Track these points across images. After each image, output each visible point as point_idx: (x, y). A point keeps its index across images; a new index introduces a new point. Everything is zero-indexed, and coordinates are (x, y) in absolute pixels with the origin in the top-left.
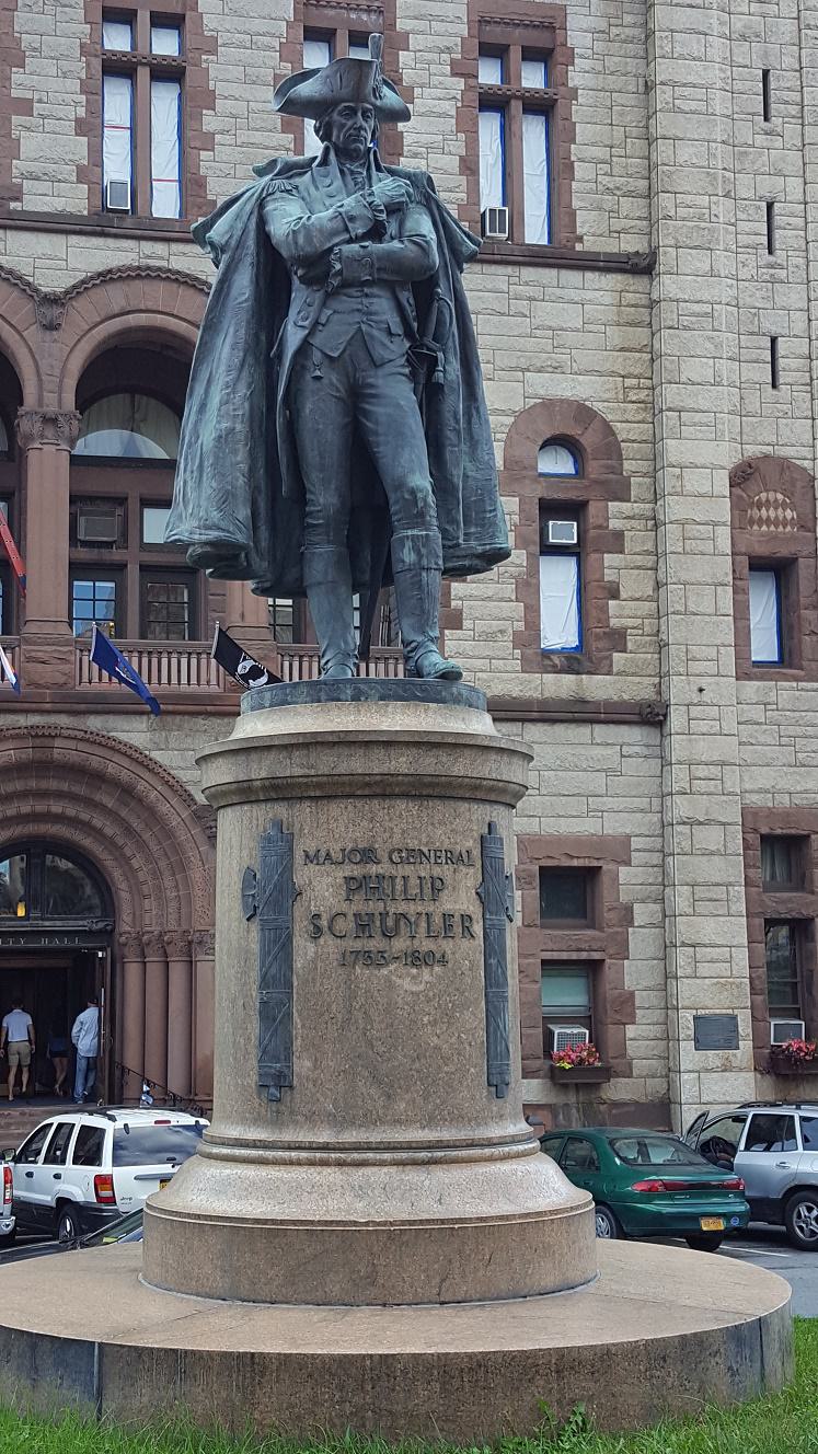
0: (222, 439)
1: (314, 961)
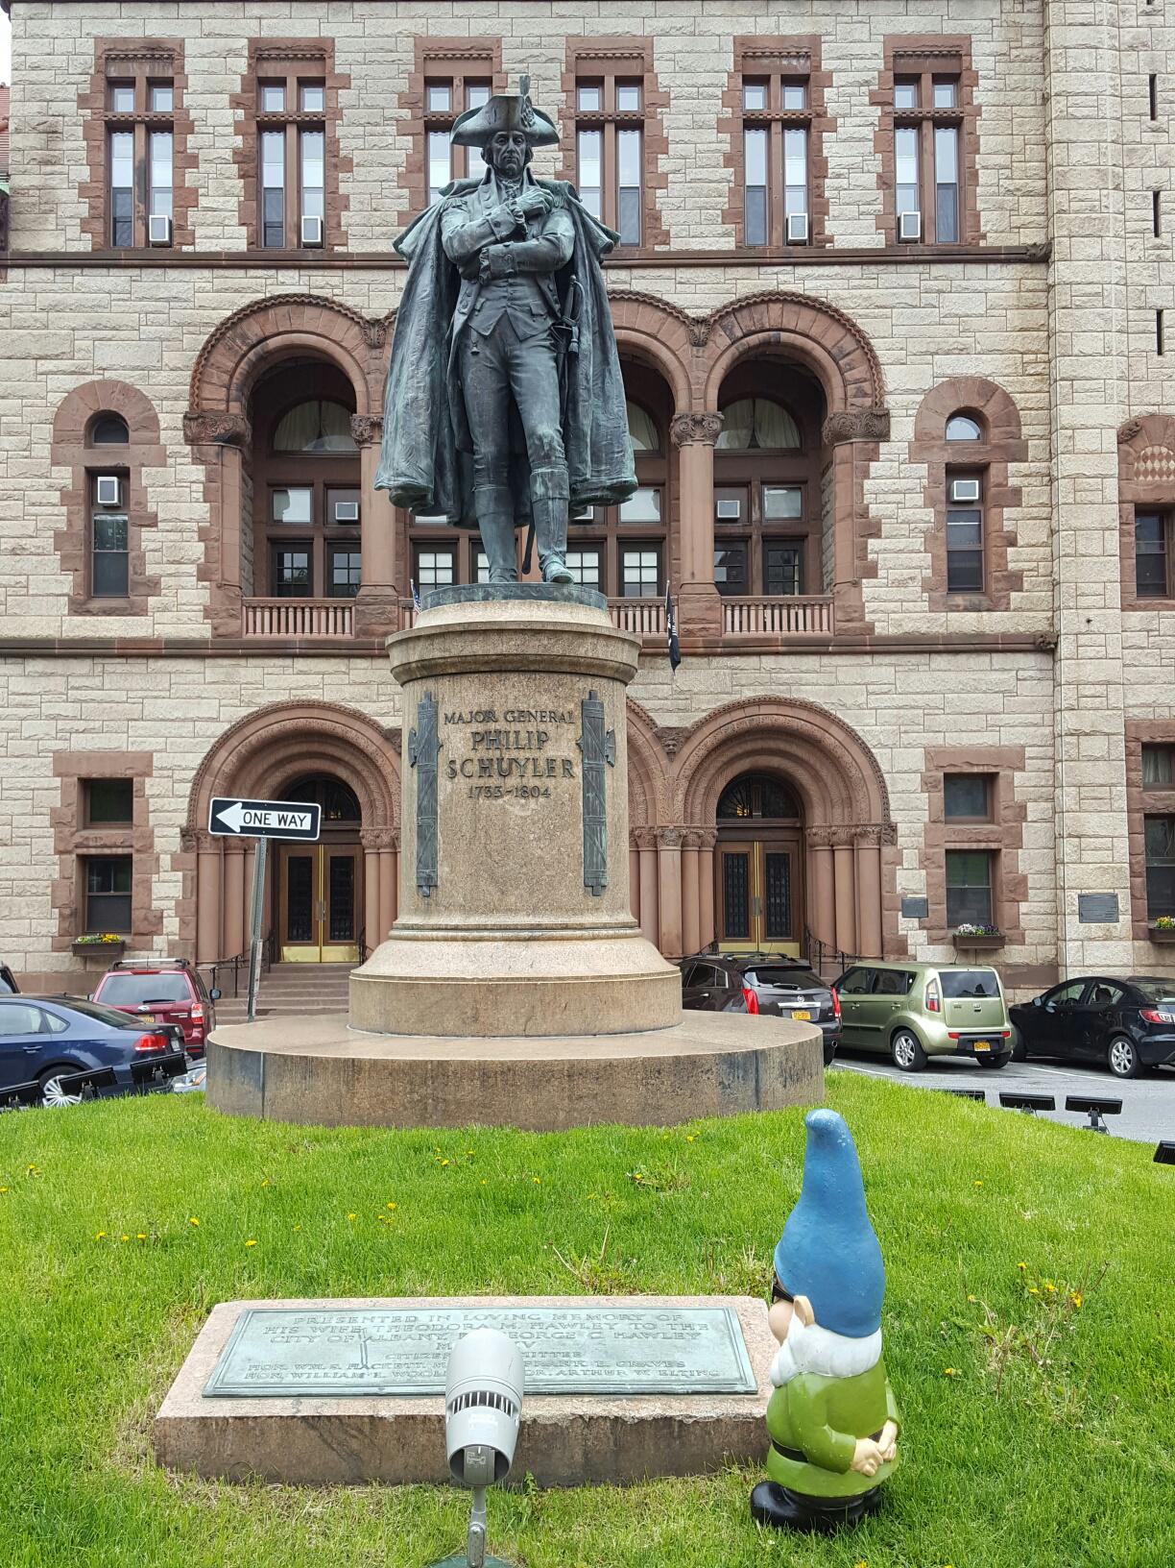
1: (451, 795)
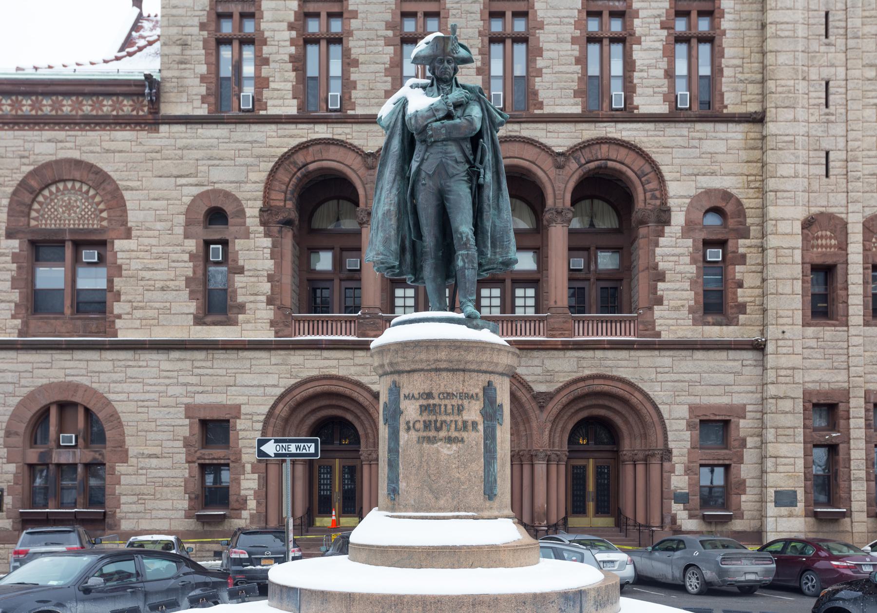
0: (387, 214)
